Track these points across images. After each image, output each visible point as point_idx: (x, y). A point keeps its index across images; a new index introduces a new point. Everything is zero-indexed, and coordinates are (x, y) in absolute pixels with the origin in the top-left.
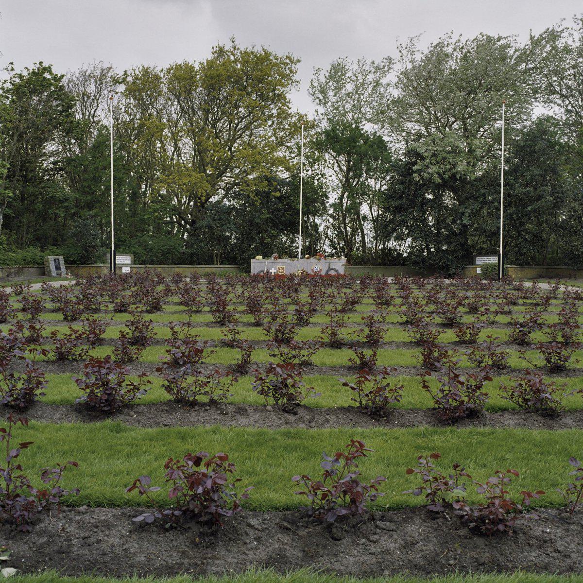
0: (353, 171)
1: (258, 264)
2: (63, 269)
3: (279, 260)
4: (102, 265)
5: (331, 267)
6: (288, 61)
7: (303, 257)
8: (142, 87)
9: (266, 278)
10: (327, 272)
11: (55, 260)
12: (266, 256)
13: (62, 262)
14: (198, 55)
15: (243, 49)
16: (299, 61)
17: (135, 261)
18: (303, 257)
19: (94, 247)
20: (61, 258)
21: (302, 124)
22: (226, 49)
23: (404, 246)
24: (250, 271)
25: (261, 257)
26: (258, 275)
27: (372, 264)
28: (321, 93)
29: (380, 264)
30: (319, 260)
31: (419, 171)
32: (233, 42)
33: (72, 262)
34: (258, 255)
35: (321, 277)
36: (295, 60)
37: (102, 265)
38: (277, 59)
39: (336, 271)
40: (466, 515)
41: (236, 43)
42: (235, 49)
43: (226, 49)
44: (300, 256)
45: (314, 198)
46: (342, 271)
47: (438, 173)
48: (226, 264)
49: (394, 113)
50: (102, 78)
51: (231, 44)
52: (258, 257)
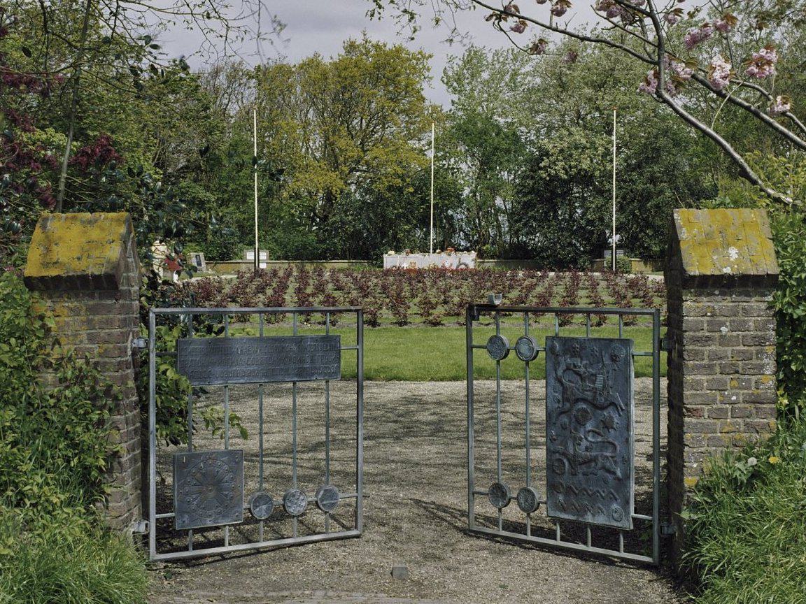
1: (392, 259)
3: (411, 255)
4: (240, 261)
5: (462, 262)
6: (420, 56)
7: (434, 252)
8: (271, 79)
9: (399, 272)
10: (458, 266)
11: (196, 256)
12: (398, 250)
13: (202, 258)
14: (330, 50)
15: (374, 42)
16: (430, 56)
17: (270, 256)
18: (434, 252)
19: (233, 244)
20: (202, 254)
21: (437, 115)
23: (538, 240)
24: (382, 267)
26: (388, 270)
27: (504, 258)
28: (455, 81)
29: (511, 258)
30: (449, 255)
31: (545, 168)
32: (365, 35)
33: (210, 259)
34: (391, 250)
35: (39, 290)
36: (427, 55)
37: (240, 261)
38: (409, 55)
39: (466, 266)
40: (381, 242)
41: (367, 36)
42: (366, 42)
44: (431, 251)
45: (449, 195)
46: (471, 266)
47: (564, 169)
49: (532, 100)
50: (235, 74)
51: (362, 37)
52: (390, 252)
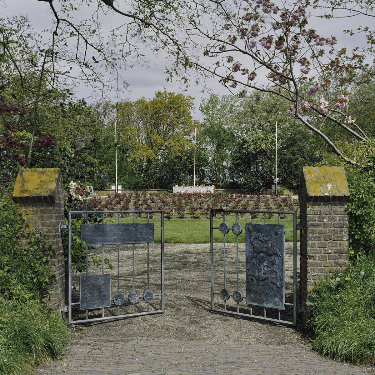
0: (219, 147)
1: (177, 189)
2: (93, 191)
3: (185, 187)
7: (196, 186)
8: (123, 108)
9: (180, 195)
12: (180, 185)
13: (92, 189)
14: (149, 96)
16: (194, 98)
18: (196, 186)
20: (92, 187)
21: (197, 125)
22: (161, 92)
23: (242, 180)
25: (177, 186)
28: (205, 110)
30: (203, 187)
33: (96, 189)
43: (161, 92)
45: (202, 160)
46: (212, 192)
47: (254, 149)
48: (296, 296)
49: (239, 118)
50: (107, 106)
51: (164, 90)
52: (176, 186)
